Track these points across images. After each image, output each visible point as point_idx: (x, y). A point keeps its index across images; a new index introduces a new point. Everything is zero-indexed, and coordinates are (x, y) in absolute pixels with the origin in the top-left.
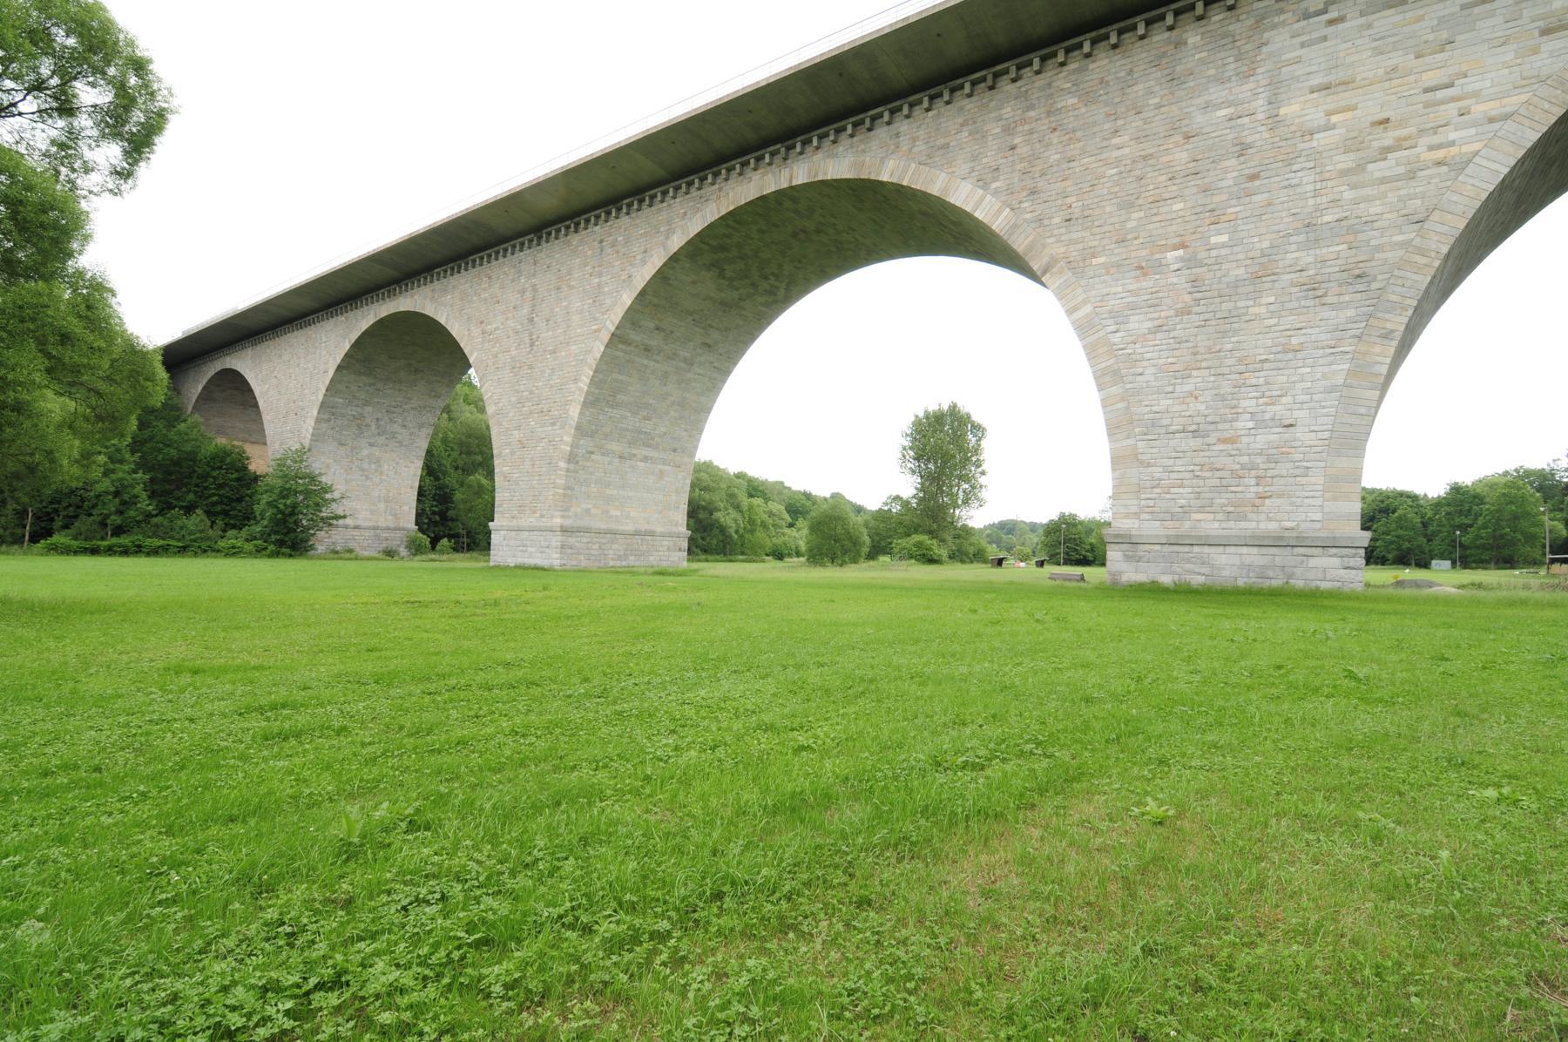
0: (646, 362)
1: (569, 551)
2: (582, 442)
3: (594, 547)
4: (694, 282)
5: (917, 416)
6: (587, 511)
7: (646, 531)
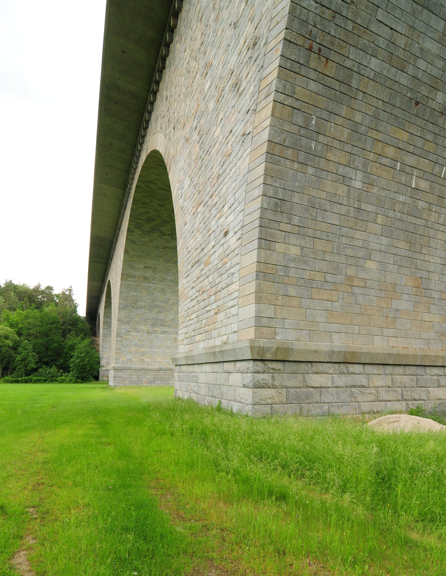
0: (148, 285)
1: (118, 379)
2: (123, 327)
3: (134, 377)
4: (151, 241)
5: (39, 286)
6: (130, 360)
7: (166, 368)
